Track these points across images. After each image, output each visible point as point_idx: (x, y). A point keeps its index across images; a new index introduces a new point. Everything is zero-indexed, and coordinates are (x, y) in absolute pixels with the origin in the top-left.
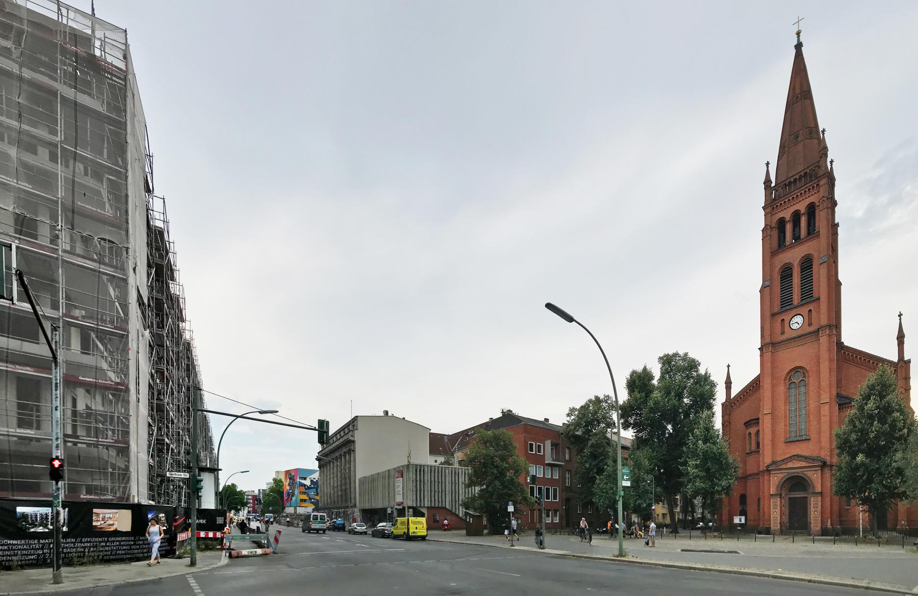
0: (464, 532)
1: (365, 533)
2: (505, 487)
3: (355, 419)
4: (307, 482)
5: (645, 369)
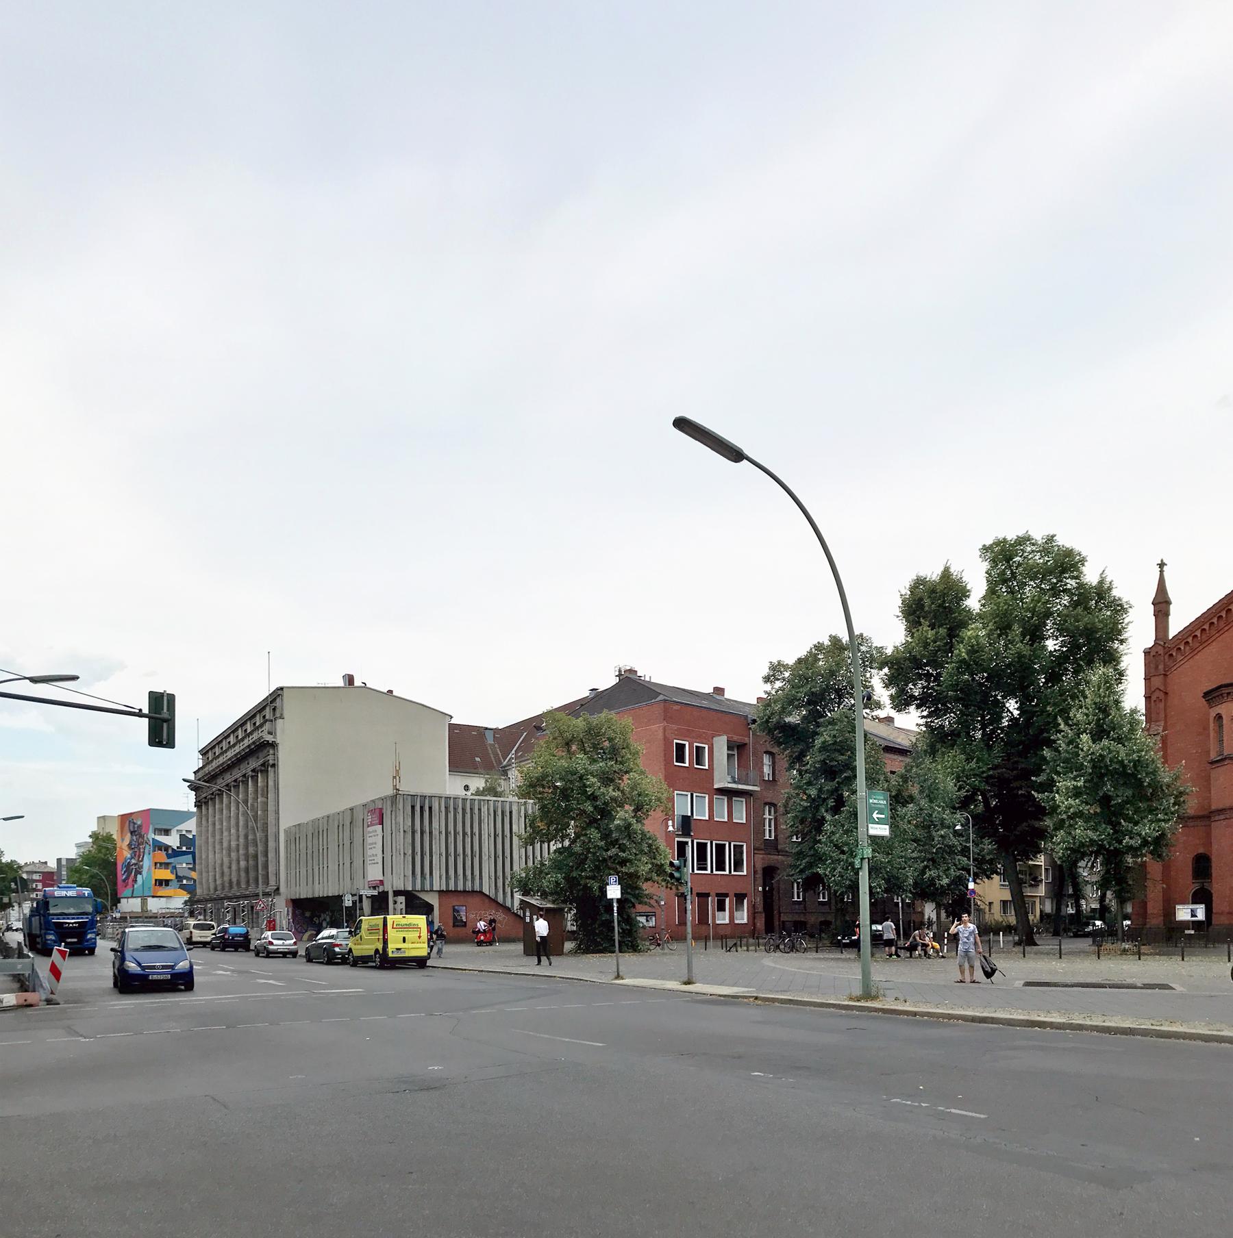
0: (520, 947)
1: (294, 954)
2: (614, 843)
3: (278, 694)
4: (173, 841)
5: (946, 573)
